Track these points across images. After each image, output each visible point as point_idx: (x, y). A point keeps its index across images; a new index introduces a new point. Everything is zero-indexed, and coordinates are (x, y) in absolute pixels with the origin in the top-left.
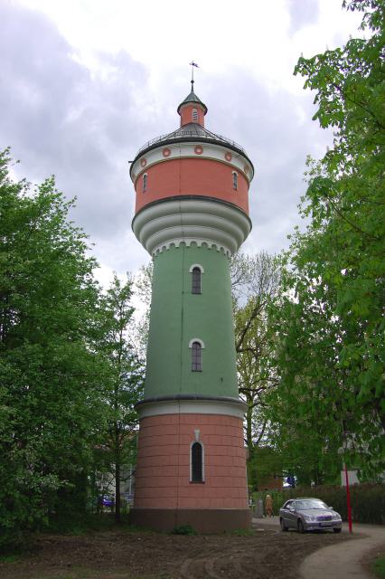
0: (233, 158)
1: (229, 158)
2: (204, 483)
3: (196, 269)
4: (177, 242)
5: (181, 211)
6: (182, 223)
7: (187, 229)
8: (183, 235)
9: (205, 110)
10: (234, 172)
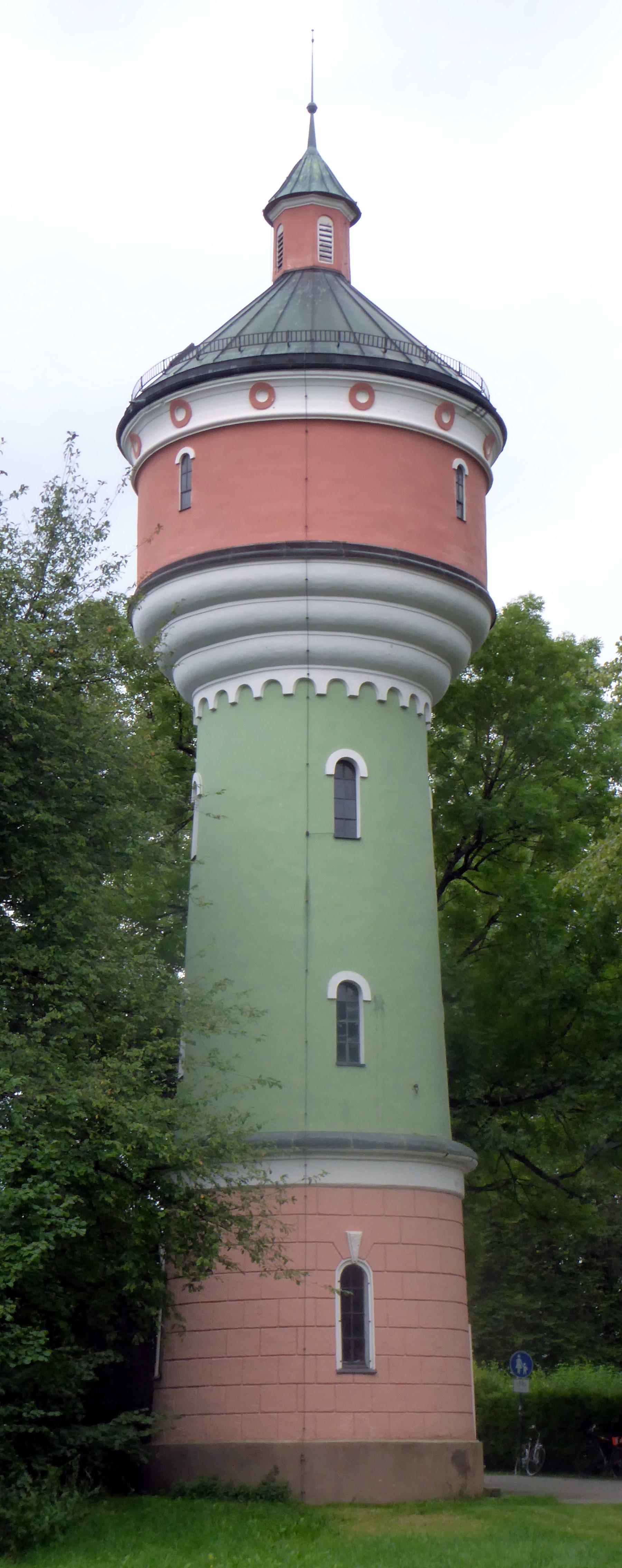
0: (458, 420)
1: (446, 419)
2: (373, 1373)
3: (346, 765)
4: (288, 678)
5: (307, 590)
6: (308, 625)
7: (322, 642)
8: (308, 659)
9: (354, 212)
10: (458, 462)
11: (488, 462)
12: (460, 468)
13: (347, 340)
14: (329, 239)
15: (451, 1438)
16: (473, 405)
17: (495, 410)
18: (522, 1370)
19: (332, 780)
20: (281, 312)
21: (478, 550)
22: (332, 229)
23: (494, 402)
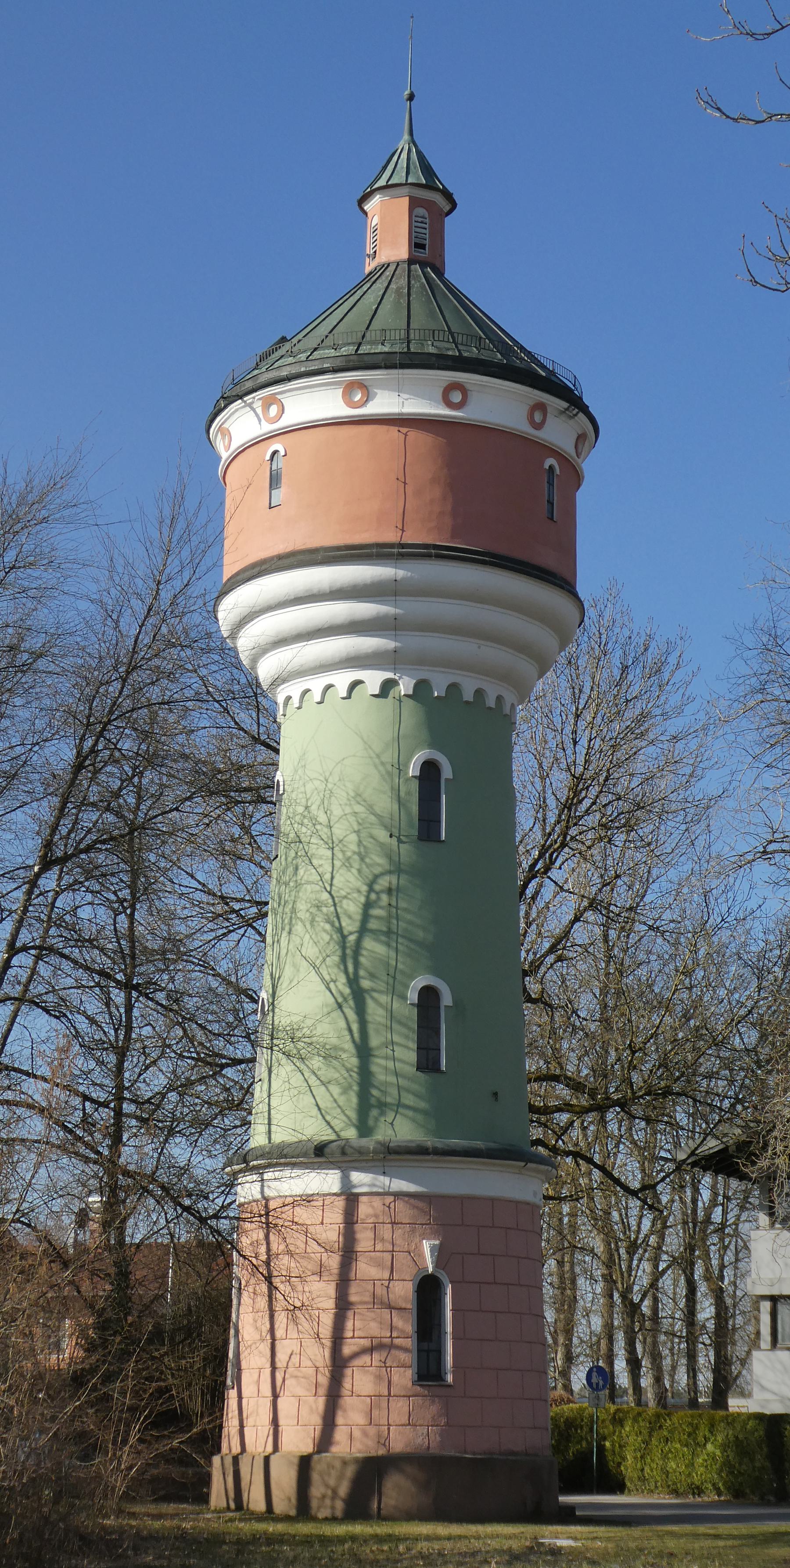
10: (550, 461)
11: (580, 461)
12: (551, 468)
13: (441, 339)
14: (423, 231)
15: (480, 1454)
16: (565, 405)
17: (588, 407)
18: (597, 1384)
19: (417, 782)
20: (374, 307)
21: (569, 551)
22: (427, 221)
23: (586, 400)
